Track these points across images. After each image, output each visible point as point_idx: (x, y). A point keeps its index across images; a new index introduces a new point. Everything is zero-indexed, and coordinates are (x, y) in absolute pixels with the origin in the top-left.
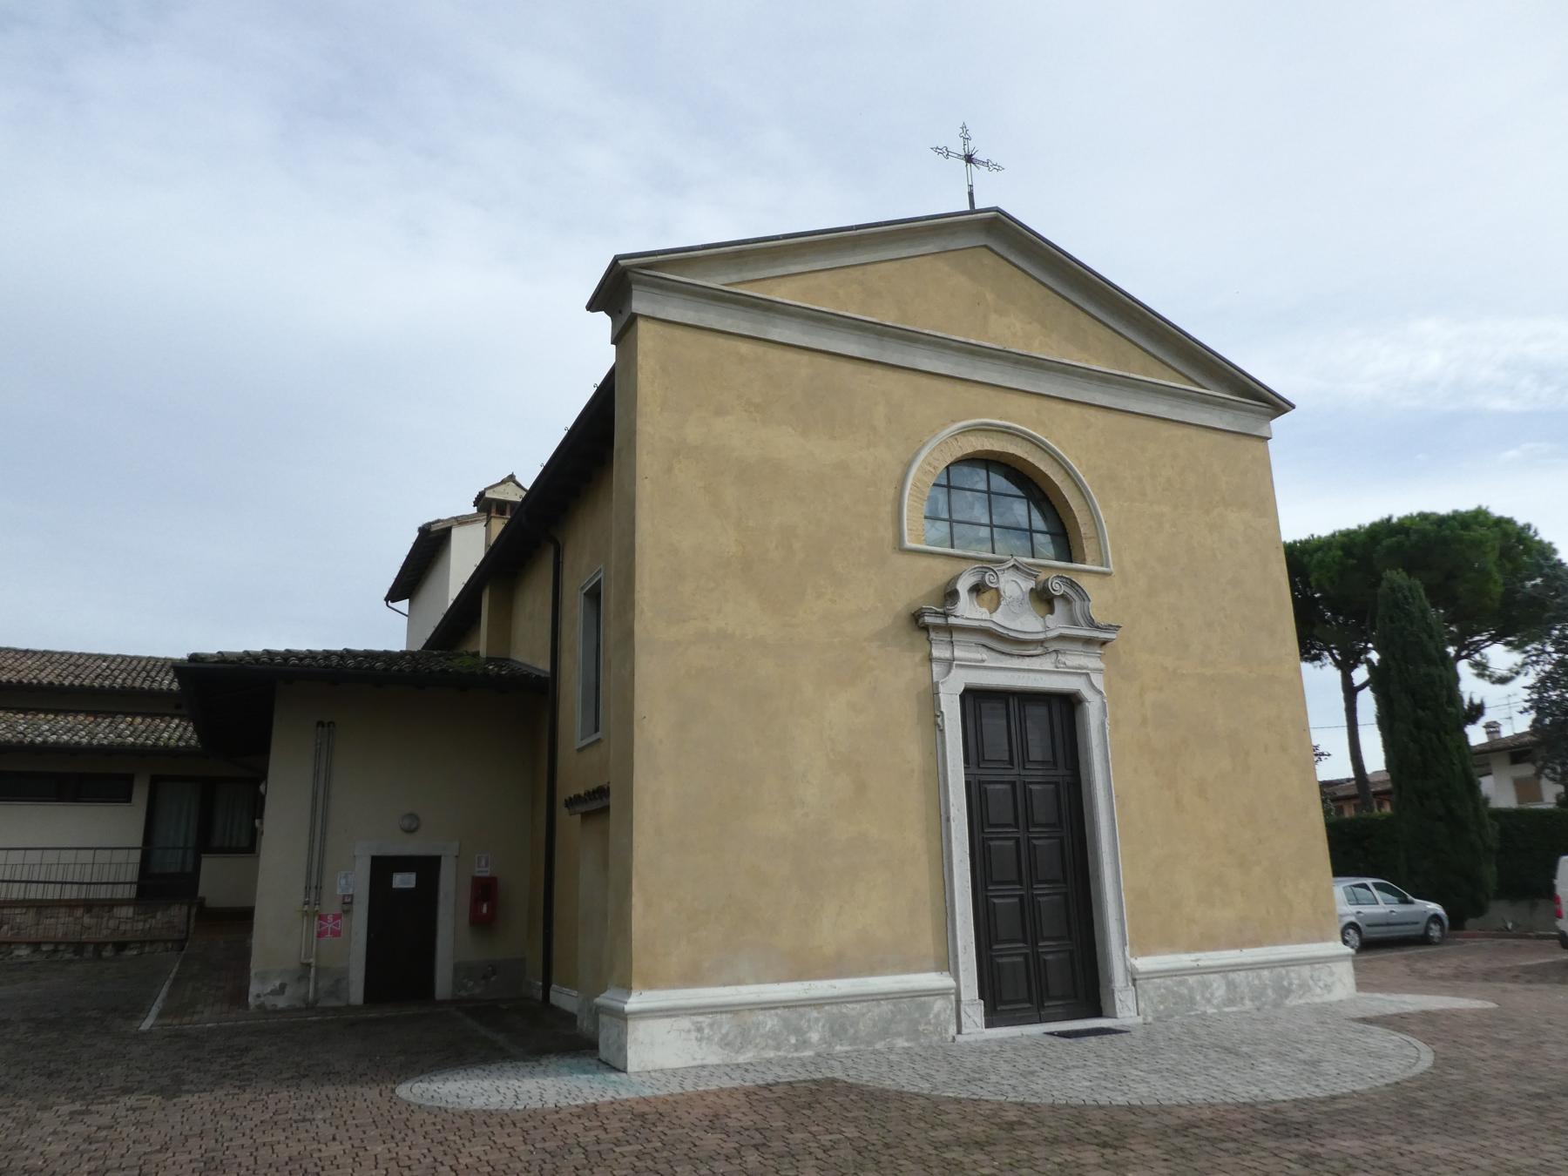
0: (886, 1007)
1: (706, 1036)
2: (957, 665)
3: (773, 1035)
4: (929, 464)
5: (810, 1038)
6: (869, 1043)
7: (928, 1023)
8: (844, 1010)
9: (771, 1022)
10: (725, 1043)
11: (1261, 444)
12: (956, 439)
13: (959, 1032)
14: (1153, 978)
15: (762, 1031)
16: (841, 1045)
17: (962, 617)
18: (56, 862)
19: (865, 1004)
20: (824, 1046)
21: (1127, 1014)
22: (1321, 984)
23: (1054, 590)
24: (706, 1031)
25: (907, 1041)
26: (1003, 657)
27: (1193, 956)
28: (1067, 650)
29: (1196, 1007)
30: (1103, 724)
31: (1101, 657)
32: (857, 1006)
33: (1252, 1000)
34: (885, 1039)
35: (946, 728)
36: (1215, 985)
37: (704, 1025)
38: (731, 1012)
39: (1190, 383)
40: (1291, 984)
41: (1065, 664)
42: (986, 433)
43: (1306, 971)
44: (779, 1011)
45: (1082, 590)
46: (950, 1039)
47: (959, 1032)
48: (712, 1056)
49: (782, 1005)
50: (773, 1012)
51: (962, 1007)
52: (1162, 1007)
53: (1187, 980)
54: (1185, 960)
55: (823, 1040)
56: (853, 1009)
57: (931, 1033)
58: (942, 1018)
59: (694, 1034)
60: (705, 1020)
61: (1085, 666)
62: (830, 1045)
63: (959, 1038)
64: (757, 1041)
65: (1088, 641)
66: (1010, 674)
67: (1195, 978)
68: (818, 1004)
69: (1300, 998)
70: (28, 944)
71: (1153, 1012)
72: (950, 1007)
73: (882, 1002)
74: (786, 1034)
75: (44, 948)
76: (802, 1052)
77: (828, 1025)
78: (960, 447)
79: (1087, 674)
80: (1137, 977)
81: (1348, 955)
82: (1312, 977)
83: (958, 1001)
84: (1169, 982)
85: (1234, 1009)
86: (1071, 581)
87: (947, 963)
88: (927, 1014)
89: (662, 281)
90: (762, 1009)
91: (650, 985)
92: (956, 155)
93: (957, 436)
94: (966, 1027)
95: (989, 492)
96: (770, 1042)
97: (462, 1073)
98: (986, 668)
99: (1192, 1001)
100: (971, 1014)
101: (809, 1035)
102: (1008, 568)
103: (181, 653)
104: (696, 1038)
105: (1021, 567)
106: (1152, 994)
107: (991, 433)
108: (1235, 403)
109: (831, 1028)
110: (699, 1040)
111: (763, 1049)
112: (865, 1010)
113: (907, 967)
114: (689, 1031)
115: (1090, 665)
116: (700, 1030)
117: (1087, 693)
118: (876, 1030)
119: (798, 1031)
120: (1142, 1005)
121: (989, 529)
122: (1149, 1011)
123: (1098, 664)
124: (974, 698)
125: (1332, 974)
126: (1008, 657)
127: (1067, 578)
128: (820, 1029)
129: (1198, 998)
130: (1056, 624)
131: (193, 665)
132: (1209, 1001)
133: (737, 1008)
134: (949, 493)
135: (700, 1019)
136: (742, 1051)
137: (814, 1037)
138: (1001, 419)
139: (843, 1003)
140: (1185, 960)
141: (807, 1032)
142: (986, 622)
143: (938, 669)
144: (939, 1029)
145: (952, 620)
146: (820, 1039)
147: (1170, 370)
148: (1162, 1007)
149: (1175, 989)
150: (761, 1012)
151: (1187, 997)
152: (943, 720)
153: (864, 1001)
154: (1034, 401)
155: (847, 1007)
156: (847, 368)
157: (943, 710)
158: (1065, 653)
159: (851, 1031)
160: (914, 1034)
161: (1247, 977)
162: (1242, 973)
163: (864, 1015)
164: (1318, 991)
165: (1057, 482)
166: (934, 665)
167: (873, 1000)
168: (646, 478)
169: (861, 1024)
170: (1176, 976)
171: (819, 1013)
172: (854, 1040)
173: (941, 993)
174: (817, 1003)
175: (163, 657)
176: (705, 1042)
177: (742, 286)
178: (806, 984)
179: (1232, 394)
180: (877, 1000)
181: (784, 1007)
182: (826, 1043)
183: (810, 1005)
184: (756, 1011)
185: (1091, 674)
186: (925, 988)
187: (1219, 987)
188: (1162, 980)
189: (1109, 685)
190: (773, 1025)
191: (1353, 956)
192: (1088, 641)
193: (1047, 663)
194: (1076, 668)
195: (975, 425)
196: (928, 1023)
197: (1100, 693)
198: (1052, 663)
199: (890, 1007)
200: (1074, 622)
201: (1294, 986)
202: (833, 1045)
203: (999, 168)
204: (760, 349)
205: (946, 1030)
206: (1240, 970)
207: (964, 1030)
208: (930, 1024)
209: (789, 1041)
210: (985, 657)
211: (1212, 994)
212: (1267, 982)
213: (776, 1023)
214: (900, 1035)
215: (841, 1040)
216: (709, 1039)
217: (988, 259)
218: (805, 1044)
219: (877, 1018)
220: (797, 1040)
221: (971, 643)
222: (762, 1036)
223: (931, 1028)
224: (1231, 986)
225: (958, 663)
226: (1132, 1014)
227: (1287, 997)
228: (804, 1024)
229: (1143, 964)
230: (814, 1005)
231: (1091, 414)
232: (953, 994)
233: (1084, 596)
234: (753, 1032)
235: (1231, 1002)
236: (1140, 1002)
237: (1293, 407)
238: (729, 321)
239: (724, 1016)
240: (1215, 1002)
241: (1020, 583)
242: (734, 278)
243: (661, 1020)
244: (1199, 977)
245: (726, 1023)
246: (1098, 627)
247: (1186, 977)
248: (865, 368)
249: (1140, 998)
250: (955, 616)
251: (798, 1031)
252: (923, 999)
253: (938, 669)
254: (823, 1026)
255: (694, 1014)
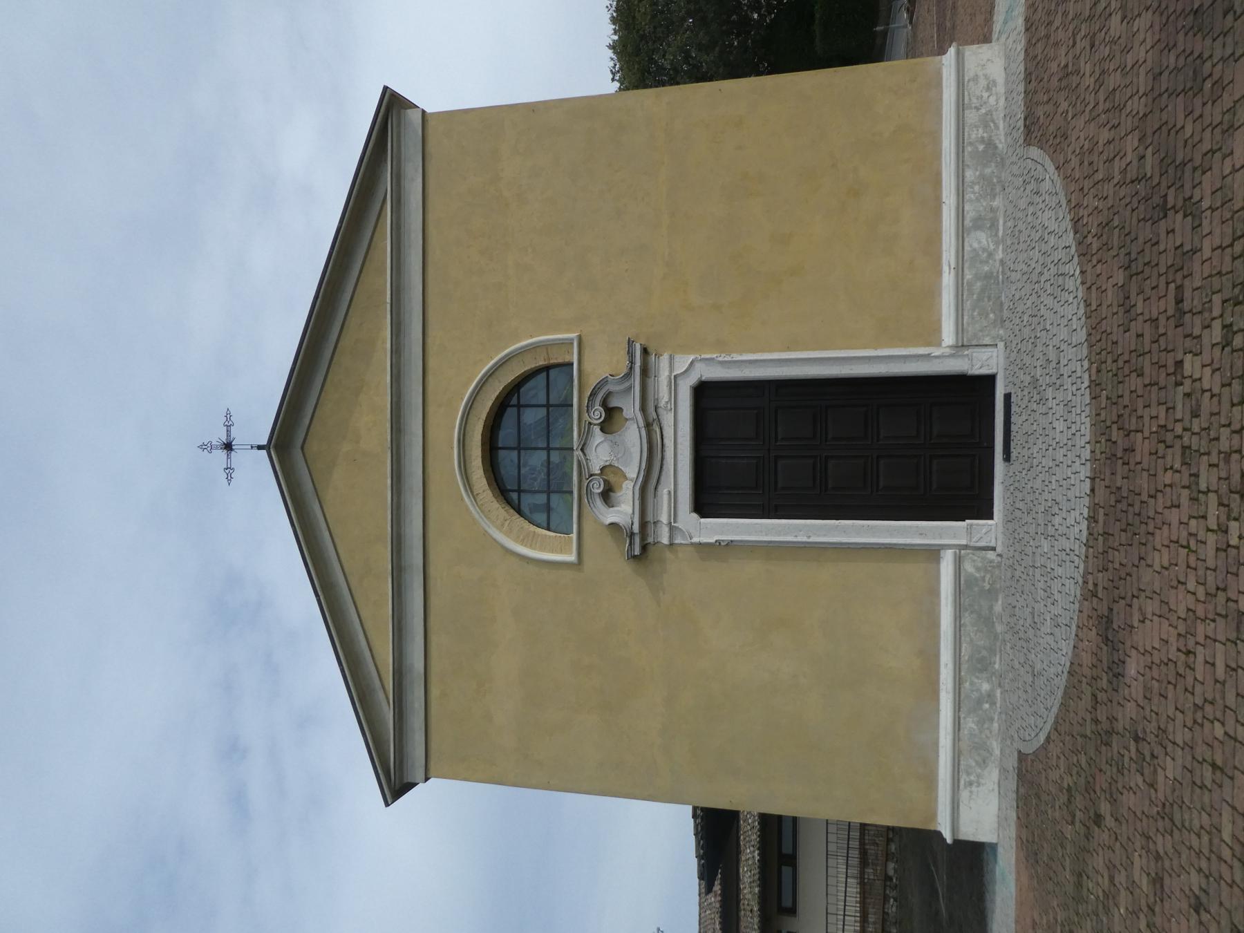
0: (967, 619)
1: (976, 778)
2: (675, 522)
3: (980, 723)
4: (503, 525)
5: (986, 691)
6: (996, 637)
7: (983, 579)
8: (967, 658)
9: (970, 724)
10: (983, 763)
11: (431, 124)
12: (477, 494)
13: (994, 549)
14: (963, 324)
15: (977, 732)
16: (995, 663)
17: (632, 519)
18: (835, 887)
19: (963, 638)
20: (994, 678)
21: (993, 362)
22: (985, 95)
23: (601, 416)
24: (972, 778)
25: (997, 600)
26: (664, 467)
27: (945, 268)
28: (654, 396)
29: (995, 271)
30: (722, 363)
31: (658, 355)
32: (964, 645)
33: (994, 197)
34: (993, 622)
35: (730, 539)
36: (976, 245)
37: (968, 780)
38: (959, 757)
39: (383, 214)
40: (982, 140)
41: (667, 402)
42: (467, 463)
43: (971, 117)
44: (962, 716)
45: (598, 384)
46: (999, 559)
47: (994, 549)
48: (992, 776)
49: (957, 712)
50: (962, 721)
51: (972, 544)
52: (992, 316)
53: (968, 280)
54: (948, 279)
55: (989, 680)
56: (966, 650)
57: (992, 576)
58: (980, 565)
59: (974, 789)
60: (964, 779)
61: (668, 379)
62: (993, 673)
63: (999, 550)
64: (984, 736)
65: (645, 372)
66: (680, 465)
67: (966, 271)
68: (959, 681)
69: (997, 127)
70: (887, 844)
71: (995, 327)
72: (971, 555)
73: (962, 622)
74: (980, 712)
75: (891, 836)
76: (997, 699)
77: (977, 674)
78: (484, 491)
79: (675, 377)
80: (960, 344)
81: (958, 53)
82: (977, 109)
83: (966, 547)
84: (968, 305)
85: (1001, 222)
86: (591, 395)
87: (932, 554)
88: (976, 579)
89: (397, 763)
90: (959, 730)
91: (933, 816)
92: (229, 460)
93: (475, 494)
94: (990, 541)
95: (519, 448)
96: (986, 726)
97: (987, 895)
98: (675, 492)
99: (988, 276)
100: (979, 536)
101: (983, 692)
102: (585, 454)
103: (697, 880)
104: (978, 787)
105: (582, 443)
106: (977, 326)
107: (467, 458)
108: (394, 163)
109: (981, 671)
110: (979, 785)
111: (991, 732)
112: (968, 639)
113: (935, 592)
114: (971, 792)
115: (667, 373)
116: (971, 784)
117: (693, 380)
118: (985, 630)
119: (979, 702)
120: (987, 341)
121: (552, 452)
122: (994, 333)
123: (664, 361)
124: (703, 506)
125: (975, 79)
126: (665, 462)
127: (589, 401)
128: (980, 681)
129: (986, 268)
130: (630, 407)
131: (706, 878)
132: (990, 255)
133: (957, 752)
134: (524, 491)
135: (962, 782)
136: (990, 750)
137: (986, 687)
138: (452, 448)
139: (960, 659)
140: (948, 279)
141: (981, 693)
142: (635, 492)
143: (679, 538)
144: (989, 569)
145: (636, 528)
146: (988, 682)
147: (375, 239)
148: (992, 316)
149: (975, 296)
150: (961, 731)
151: (985, 282)
152: (723, 541)
153: (960, 638)
154: (431, 409)
155: (964, 655)
156: (434, 601)
157: (712, 540)
158: (657, 399)
159: (984, 653)
160: (992, 593)
161: (971, 201)
162: (967, 208)
163: (971, 640)
164: (992, 100)
165: (501, 388)
166: (676, 542)
167: (960, 630)
168: (549, 782)
169: (979, 643)
170: (962, 295)
171: (966, 681)
172: (992, 651)
173: (958, 561)
174: (958, 682)
175: (696, 860)
176: (981, 780)
177: (386, 684)
178: (942, 687)
179: (386, 239)
180: (960, 626)
181: (959, 711)
182: (991, 677)
183: (960, 689)
184: (961, 735)
185: (675, 373)
186: (953, 581)
187: (979, 240)
188: (965, 313)
189: (686, 349)
190: (973, 722)
191: (959, 45)
192: (645, 372)
193: (667, 419)
194: (670, 388)
195: (462, 478)
196: (983, 579)
197: (692, 363)
198: (667, 414)
199: (967, 615)
200: (629, 389)
201: (985, 135)
202: (994, 671)
203: (228, 416)
204: (433, 679)
205: (991, 561)
206: (963, 211)
207: (993, 544)
208: (984, 577)
209: (987, 710)
210: (665, 491)
211: (984, 250)
212: (978, 173)
213: (971, 719)
214: (991, 608)
215: (990, 664)
216: (979, 776)
217: (313, 446)
218: (990, 696)
219: (976, 628)
220: (987, 702)
221: (654, 501)
222: (981, 732)
223: (988, 576)
224: (978, 224)
225: (672, 521)
226: (995, 354)
227: (996, 148)
228: (975, 695)
229: (948, 336)
230: (960, 684)
231: (432, 348)
232: (960, 552)
233: (604, 382)
234: (976, 740)
235: (994, 225)
236: (985, 343)
237: (386, 88)
238: (416, 705)
239: (962, 762)
240: (992, 247)
241: (596, 444)
242: (381, 695)
243: (961, 813)
244: (966, 265)
245: (967, 761)
246: (631, 368)
247: (965, 281)
248: (431, 583)
249: (981, 342)
250: (632, 524)
251: (979, 702)
252: (962, 582)
253: (679, 538)
254: (978, 678)
255: (959, 786)
